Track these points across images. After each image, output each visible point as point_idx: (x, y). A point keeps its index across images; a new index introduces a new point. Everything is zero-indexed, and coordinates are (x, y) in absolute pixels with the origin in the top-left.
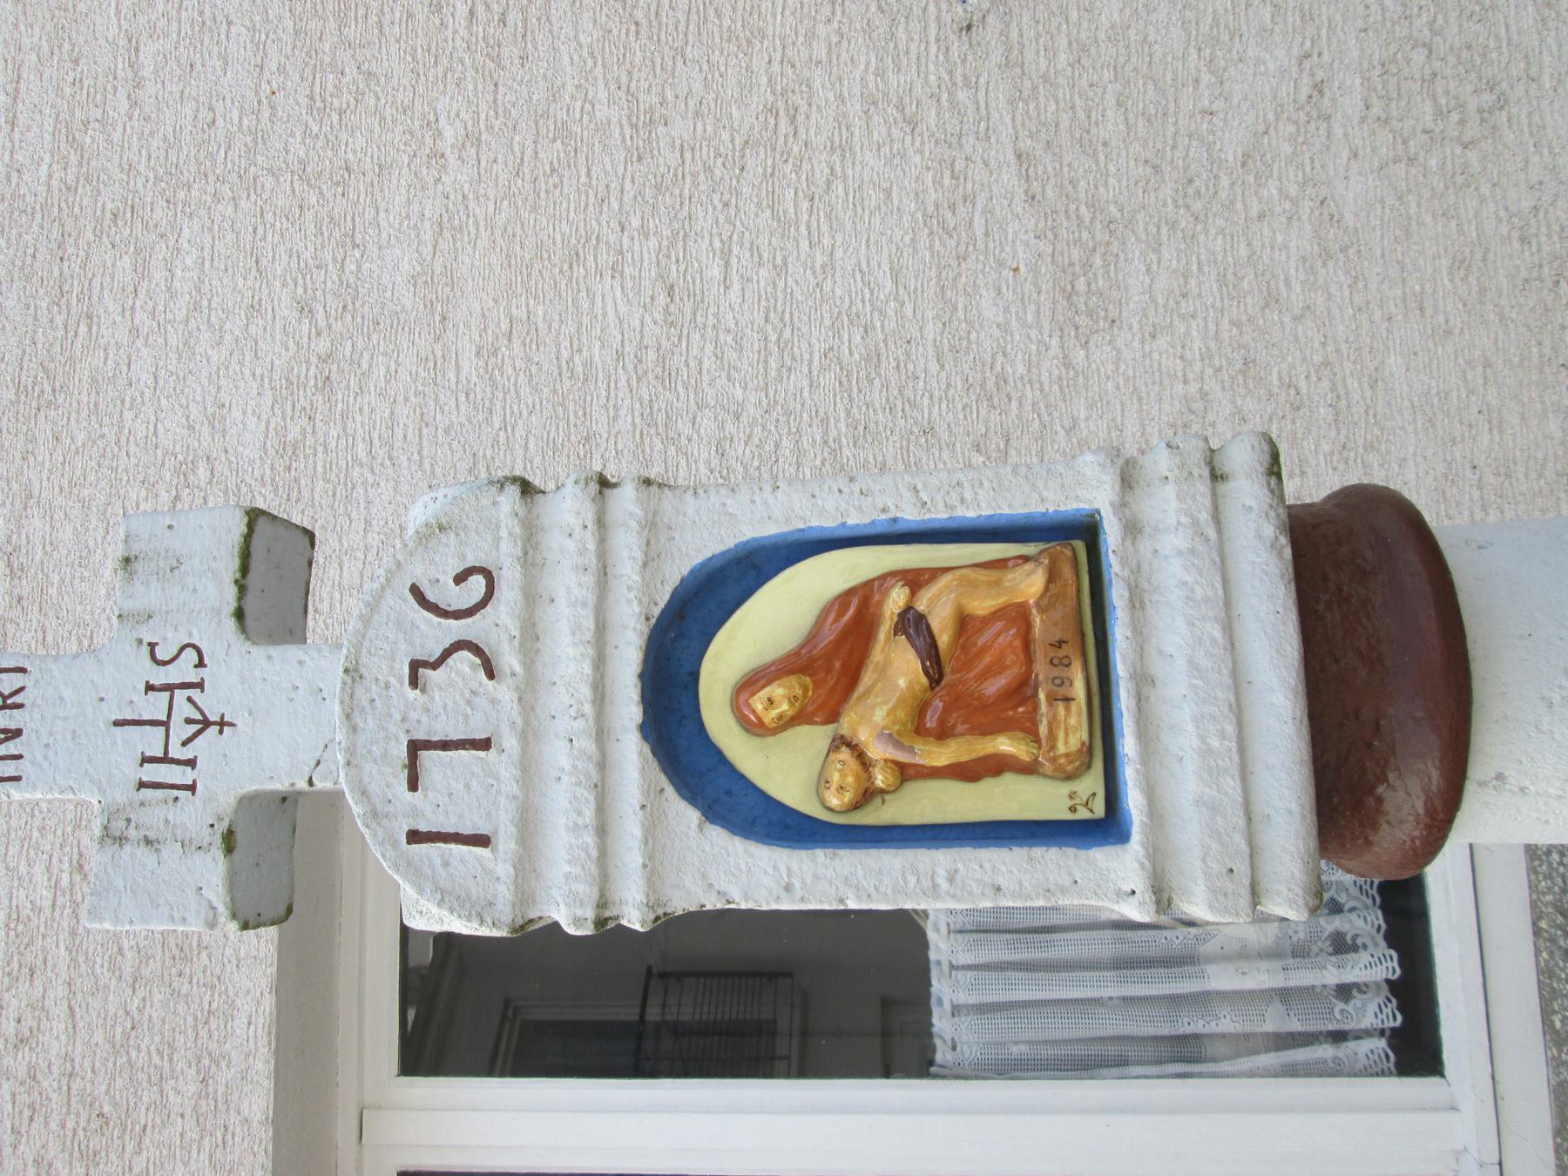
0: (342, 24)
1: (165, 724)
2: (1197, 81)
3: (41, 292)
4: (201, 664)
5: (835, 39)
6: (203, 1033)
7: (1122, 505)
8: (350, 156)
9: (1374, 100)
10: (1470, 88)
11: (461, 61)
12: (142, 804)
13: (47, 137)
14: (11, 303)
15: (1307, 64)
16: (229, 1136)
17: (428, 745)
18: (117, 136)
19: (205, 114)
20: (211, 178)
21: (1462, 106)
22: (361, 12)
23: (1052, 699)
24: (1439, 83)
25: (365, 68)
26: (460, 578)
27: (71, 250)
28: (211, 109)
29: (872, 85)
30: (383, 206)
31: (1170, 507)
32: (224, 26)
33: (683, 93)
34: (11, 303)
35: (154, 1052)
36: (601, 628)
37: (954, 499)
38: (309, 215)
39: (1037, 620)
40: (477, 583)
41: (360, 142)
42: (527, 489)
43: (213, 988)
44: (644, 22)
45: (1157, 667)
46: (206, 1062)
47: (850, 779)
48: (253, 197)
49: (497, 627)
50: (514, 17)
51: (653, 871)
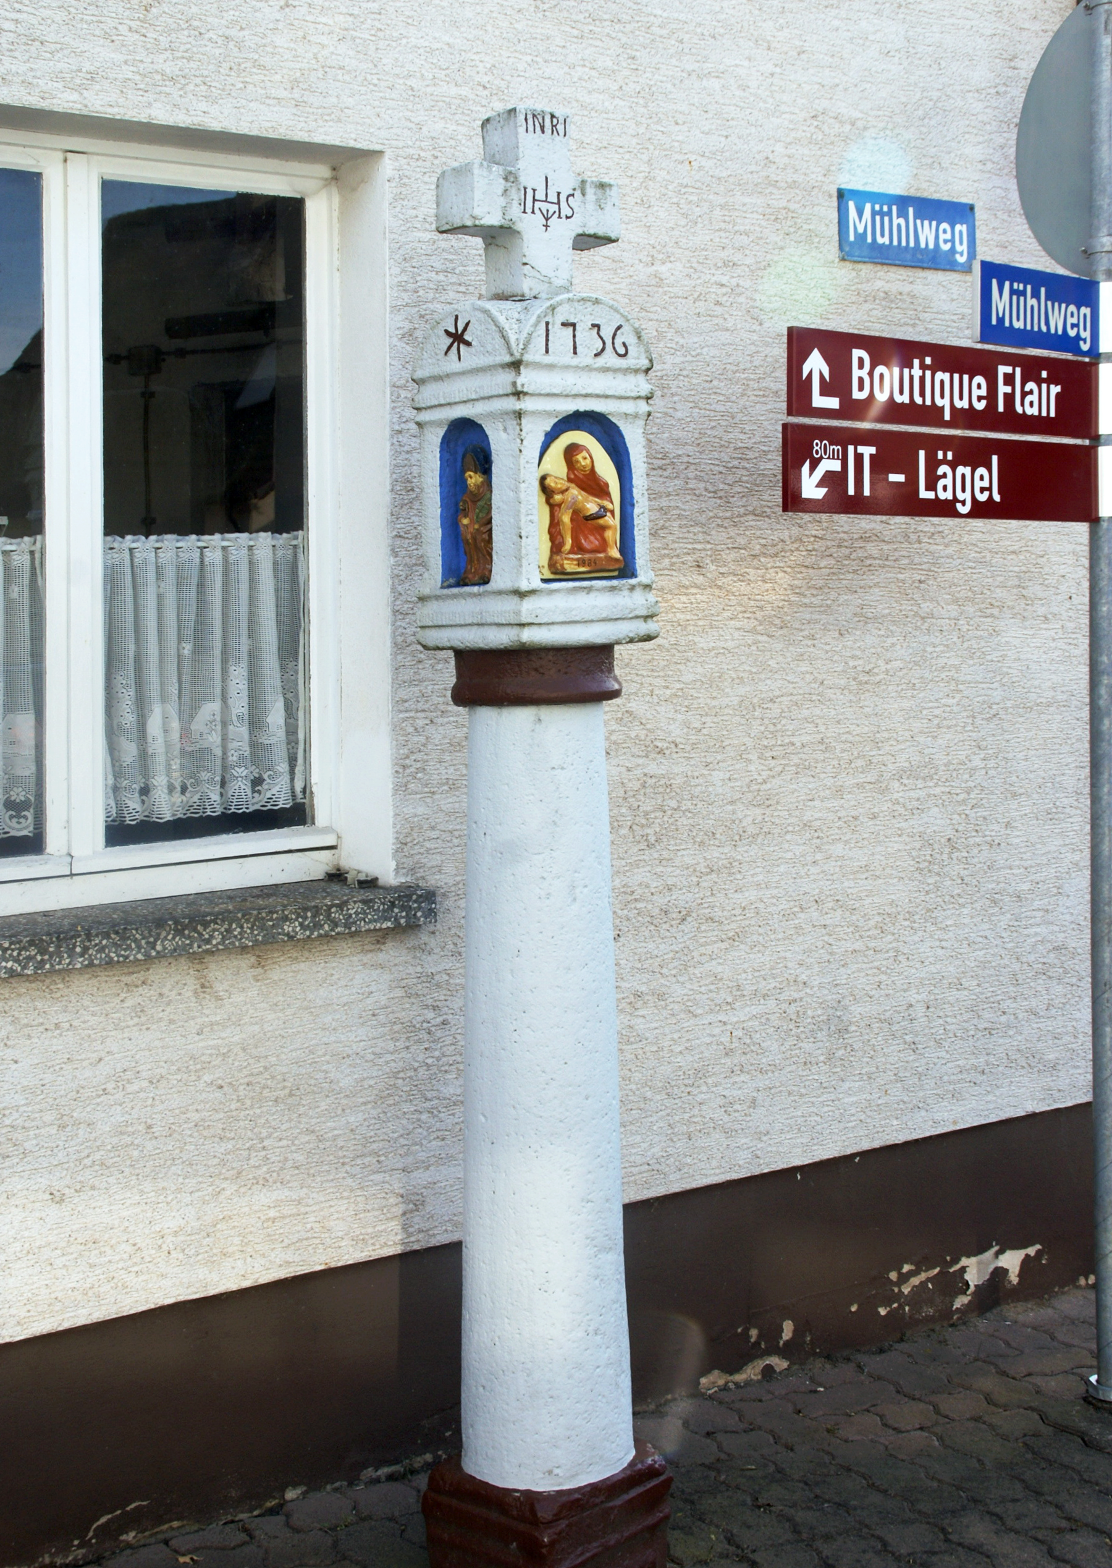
0: (722, 207)
1: (546, 201)
2: (667, 687)
3: (596, 6)
4: (567, 217)
5: (697, 492)
6: (198, 81)
7: (640, 584)
8: (656, 208)
9: (654, 780)
10: (658, 830)
11: (699, 278)
13: (676, 15)
15: (673, 746)
16: (141, 93)
17: (574, 330)
18: (674, 61)
20: (649, 121)
21: (649, 826)
22: (727, 219)
23: (578, 560)
24: (661, 814)
26: (624, 344)
27: (617, 27)
28: (684, 123)
29: (674, 512)
30: (629, 227)
31: (639, 601)
32: (725, 134)
33: (678, 406)
35: (189, 46)
36: (607, 397)
37: (640, 527)
38: (627, 181)
39: (602, 555)
40: (622, 351)
42: (647, 371)
43: (223, 90)
44: (711, 385)
45: (593, 595)
46: (183, 81)
48: (639, 147)
49: (609, 359)
50: (719, 310)
51: (533, 413)
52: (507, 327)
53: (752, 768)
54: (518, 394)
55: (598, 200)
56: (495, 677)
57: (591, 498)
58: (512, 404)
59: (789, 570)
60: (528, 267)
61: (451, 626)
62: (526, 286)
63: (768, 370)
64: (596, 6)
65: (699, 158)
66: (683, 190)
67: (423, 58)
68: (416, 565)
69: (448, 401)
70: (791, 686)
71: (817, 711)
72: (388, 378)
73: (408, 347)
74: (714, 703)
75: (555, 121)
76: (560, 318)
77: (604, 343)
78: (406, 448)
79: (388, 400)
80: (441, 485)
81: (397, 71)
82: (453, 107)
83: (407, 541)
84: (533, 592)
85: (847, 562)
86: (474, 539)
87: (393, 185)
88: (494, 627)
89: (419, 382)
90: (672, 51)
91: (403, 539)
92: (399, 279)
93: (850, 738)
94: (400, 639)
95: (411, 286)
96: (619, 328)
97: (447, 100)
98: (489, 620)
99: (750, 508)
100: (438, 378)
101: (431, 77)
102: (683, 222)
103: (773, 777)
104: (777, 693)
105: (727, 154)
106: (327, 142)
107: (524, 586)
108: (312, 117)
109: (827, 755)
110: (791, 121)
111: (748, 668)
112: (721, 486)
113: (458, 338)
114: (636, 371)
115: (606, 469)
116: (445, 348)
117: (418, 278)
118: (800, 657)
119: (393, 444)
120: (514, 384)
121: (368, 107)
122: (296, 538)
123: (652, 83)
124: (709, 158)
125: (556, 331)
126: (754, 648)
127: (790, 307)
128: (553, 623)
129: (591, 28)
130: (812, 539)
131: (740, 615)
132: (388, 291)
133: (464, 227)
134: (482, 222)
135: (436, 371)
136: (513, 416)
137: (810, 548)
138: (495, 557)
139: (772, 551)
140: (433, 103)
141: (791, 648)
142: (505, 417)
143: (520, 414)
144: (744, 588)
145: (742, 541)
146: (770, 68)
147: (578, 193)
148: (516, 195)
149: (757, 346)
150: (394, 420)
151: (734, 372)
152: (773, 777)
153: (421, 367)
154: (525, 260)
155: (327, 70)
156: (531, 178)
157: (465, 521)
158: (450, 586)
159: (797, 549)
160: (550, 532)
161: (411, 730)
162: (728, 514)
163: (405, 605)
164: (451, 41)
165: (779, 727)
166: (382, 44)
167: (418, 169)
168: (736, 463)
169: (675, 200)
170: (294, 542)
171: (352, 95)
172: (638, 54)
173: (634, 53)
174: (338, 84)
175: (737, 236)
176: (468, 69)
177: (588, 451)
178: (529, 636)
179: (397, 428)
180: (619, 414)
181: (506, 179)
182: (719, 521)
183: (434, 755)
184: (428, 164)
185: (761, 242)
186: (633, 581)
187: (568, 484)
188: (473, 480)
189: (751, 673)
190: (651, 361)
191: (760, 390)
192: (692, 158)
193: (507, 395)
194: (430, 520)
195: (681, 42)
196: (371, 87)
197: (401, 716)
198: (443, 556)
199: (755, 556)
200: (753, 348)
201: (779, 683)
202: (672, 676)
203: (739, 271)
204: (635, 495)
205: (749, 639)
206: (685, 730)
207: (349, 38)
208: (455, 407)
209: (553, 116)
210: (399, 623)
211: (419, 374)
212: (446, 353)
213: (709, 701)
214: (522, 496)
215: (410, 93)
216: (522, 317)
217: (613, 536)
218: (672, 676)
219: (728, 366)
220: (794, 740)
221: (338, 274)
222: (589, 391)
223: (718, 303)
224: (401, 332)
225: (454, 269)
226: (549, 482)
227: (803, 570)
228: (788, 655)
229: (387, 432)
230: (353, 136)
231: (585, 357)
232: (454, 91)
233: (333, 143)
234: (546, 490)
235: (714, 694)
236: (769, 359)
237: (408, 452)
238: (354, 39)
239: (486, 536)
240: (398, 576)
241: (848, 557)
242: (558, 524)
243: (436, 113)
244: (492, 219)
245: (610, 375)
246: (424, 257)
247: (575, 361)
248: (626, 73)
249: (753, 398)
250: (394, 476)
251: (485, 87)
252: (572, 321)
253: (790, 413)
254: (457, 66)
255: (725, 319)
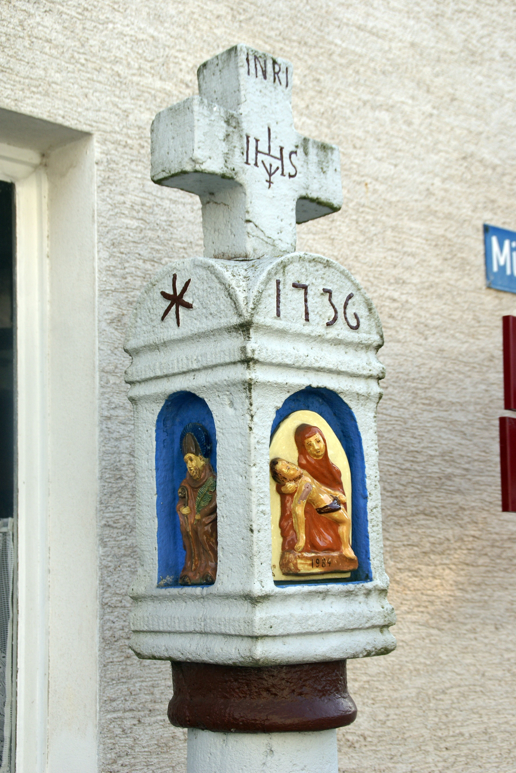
0: (394, 228)
1: (269, 154)
4: (290, 176)
8: (338, 223)
11: (375, 291)
12: (241, 136)
14: (281, 5)
15: (362, 739)
17: (306, 294)
18: (351, 90)
19: (358, 144)
22: (397, 240)
23: (311, 559)
25: (375, 238)
28: (361, 148)
30: (317, 237)
31: (373, 608)
34: (281, 5)
36: (339, 373)
39: (335, 554)
40: (354, 323)
41: (344, 229)
45: (328, 600)
47: (292, 472)
49: (341, 330)
51: (265, 385)
52: (233, 283)
53: (429, 759)
54: (248, 361)
55: (320, 162)
56: (218, 697)
57: (323, 488)
58: (241, 373)
59: (453, 567)
60: (251, 224)
61: (170, 632)
62: (250, 245)
63: (433, 381)
64: (286, 26)
65: (374, 182)
66: (361, 210)
67: (129, 46)
68: (124, 555)
69: (166, 372)
70: (459, 677)
71: (481, 703)
72: (97, 363)
73: (116, 333)
74: (396, 695)
75: (277, 69)
76: (291, 279)
77: (336, 312)
78: (115, 435)
79: (97, 385)
80: (157, 469)
81: (105, 54)
82: (159, 100)
83: (116, 531)
84: (266, 597)
85: (498, 561)
86: (196, 532)
87: (101, 168)
88: (220, 637)
89: (132, 353)
90: (350, 80)
91: (113, 529)
92: (108, 263)
93: (508, 729)
94: (108, 634)
95: (119, 272)
96: (350, 297)
97: (153, 92)
98: (214, 629)
99: (421, 508)
100: (154, 347)
101: (136, 66)
102: (361, 238)
103: (448, 768)
104: (448, 685)
105: (396, 181)
106: (35, 115)
107: (257, 590)
108: (19, 86)
109: (491, 745)
110: (446, 159)
111: (423, 660)
112: (397, 486)
113: (176, 300)
114: (367, 347)
115: (338, 457)
116: (162, 312)
117: (127, 265)
118: (465, 650)
119: (102, 430)
120: (243, 349)
121: (76, 86)
122: (6, 525)
123: (334, 106)
124: (382, 183)
125: (287, 290)
126: (427, 641)
127: (449, 326)
128: (288, 635)
129: (281, 45)
130: (471, 539)
131: (415, 610)
132: (97, 275)
133: (184, 173)
134: (203, 167)
135: (152, 339)
136: (241, 388)
137: (470, 546)
138: (220, 554)
139: (440, 549)
140: (139, 93)
141: (458, 642)
142: (232, 389)
143: (250, 385)
144: (416, 582)
145: (415, 538)
146: (428, 108)
147: (300, 151)
148: (238, 143)
149: (423, 358)
150: (104, 406)
151: (406, 381)
152: (448, 768)
153: (135, 335)
154: (248, 217)
155: (34, 40)
156: (254, 127)
157: (185, 511)
158: (167, 586)
159: (460, 548)
160: (281, 526)
161: (118, 731)
162: (403, 513)
163: (114, 602)
164: (156, 34)
165: (450, 718)
166: (89, 25)
167: (125, 156)
168: (408, 465)
169: (354, 217)
170: (4, 530)
171: (59, 71)
172: (322, 78)
173: (318, 76)
174: (46, 57)
175: (405, 257)
176: (171, 65)
177: (321, 435)
178: (266, 651)
179: (106, 414)
180: (351, 393)
181: (228, 122)
182: (396, 519)
183: (141, 758)
184: (135, 152)
185: (425, 264)
186: (369, 585)
187: (300, 470)
188: (194, 464)
189: (426, 665)
190: (382, 337)
191: (426, 398)
192: (369, 180)
193: (234, 363)
194: (145, 509)
195: (357, 72)
196: (79, 66)
197: (109, 716)
198: (160, 549)
199: (425, 553)
200: (419, 360)
201: (449, 675)
202: (360, 669)
203: (407, 289)
204: (368, 486)
205: (424, 631)
206: (372, 723)
207: (56, 11)
208: (173, 379)
209: (274, 62)
210: (107, 617)
211: (132, 344)
212: (163, 319)
213: (391, 693)
214: (253, 481)
215: (117, 79)
216: (250, 274)
217: (345, 532)
218: (360, 669)
219: (401, 375)
220: (464, 730)
221: (47, 261)
222: (322, 364)
223: (391, 316)
224: (110, 317)
225: (160, 259)
226: (280, 466)
227: (465, 567)
228: (455, 647)
229: (97, 418)
230: (61, 112)
231: (317, 327)
232: (158, 84)
233: (40, 116)
234: (276, 475)
235: (396, 686)
236: (433, 372)
237: (117, 439)
238: (61, 13)
239: (208, 528)
240: (107, 567)
241: (499, 557)
242: (290, 516)
243: (142, 103)
244: (214, 165)
245: (341, 349)
246: (131, 244)
247: (307, 329)
248: (312, 93)
249: (421, 406)
250: (104, 463)
251: (187, 86)
252: (303, 282)
253: (507, 406)
254: (161, 60)
255: (397, 332)
